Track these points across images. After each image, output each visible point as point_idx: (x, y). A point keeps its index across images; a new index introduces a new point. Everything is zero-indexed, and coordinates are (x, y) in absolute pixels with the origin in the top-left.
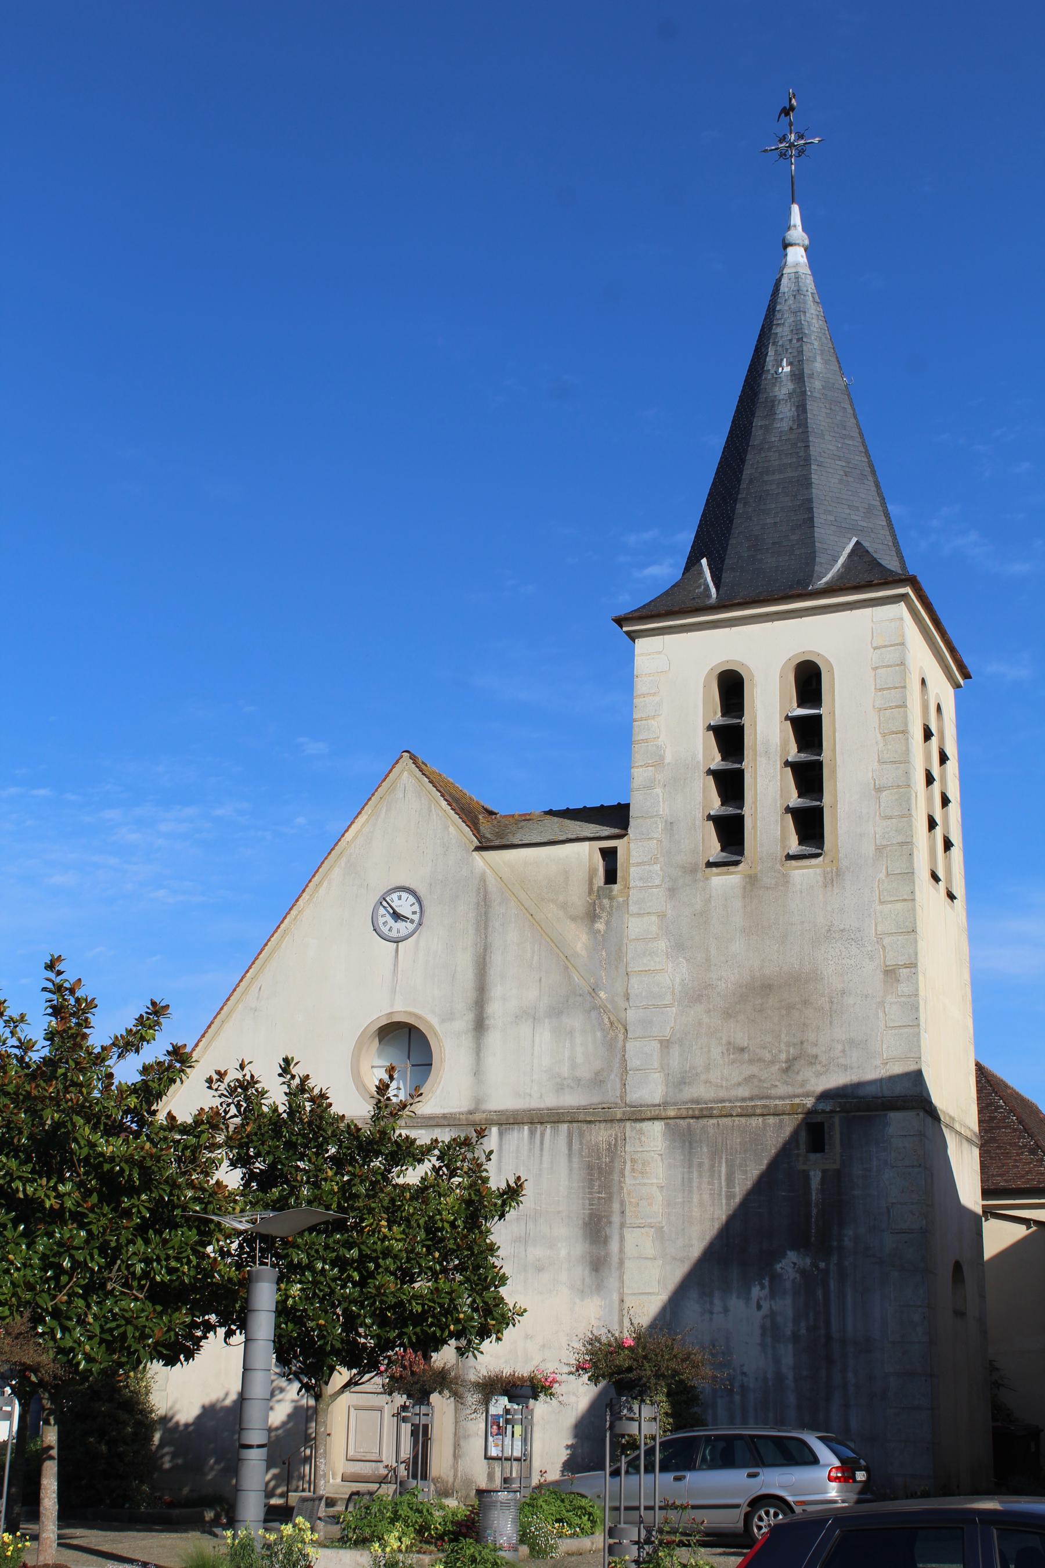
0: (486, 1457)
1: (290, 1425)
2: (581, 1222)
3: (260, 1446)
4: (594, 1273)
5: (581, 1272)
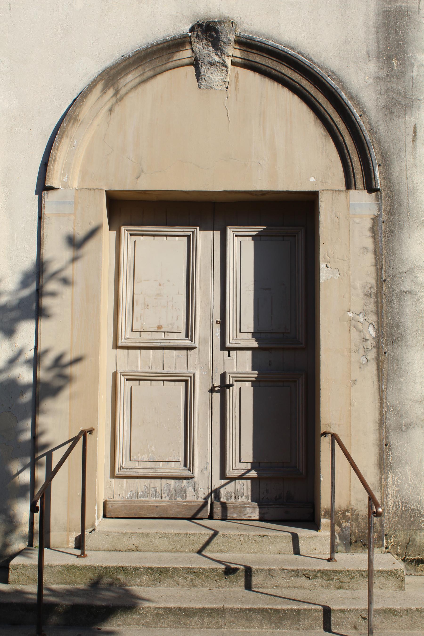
3: (18, 473)
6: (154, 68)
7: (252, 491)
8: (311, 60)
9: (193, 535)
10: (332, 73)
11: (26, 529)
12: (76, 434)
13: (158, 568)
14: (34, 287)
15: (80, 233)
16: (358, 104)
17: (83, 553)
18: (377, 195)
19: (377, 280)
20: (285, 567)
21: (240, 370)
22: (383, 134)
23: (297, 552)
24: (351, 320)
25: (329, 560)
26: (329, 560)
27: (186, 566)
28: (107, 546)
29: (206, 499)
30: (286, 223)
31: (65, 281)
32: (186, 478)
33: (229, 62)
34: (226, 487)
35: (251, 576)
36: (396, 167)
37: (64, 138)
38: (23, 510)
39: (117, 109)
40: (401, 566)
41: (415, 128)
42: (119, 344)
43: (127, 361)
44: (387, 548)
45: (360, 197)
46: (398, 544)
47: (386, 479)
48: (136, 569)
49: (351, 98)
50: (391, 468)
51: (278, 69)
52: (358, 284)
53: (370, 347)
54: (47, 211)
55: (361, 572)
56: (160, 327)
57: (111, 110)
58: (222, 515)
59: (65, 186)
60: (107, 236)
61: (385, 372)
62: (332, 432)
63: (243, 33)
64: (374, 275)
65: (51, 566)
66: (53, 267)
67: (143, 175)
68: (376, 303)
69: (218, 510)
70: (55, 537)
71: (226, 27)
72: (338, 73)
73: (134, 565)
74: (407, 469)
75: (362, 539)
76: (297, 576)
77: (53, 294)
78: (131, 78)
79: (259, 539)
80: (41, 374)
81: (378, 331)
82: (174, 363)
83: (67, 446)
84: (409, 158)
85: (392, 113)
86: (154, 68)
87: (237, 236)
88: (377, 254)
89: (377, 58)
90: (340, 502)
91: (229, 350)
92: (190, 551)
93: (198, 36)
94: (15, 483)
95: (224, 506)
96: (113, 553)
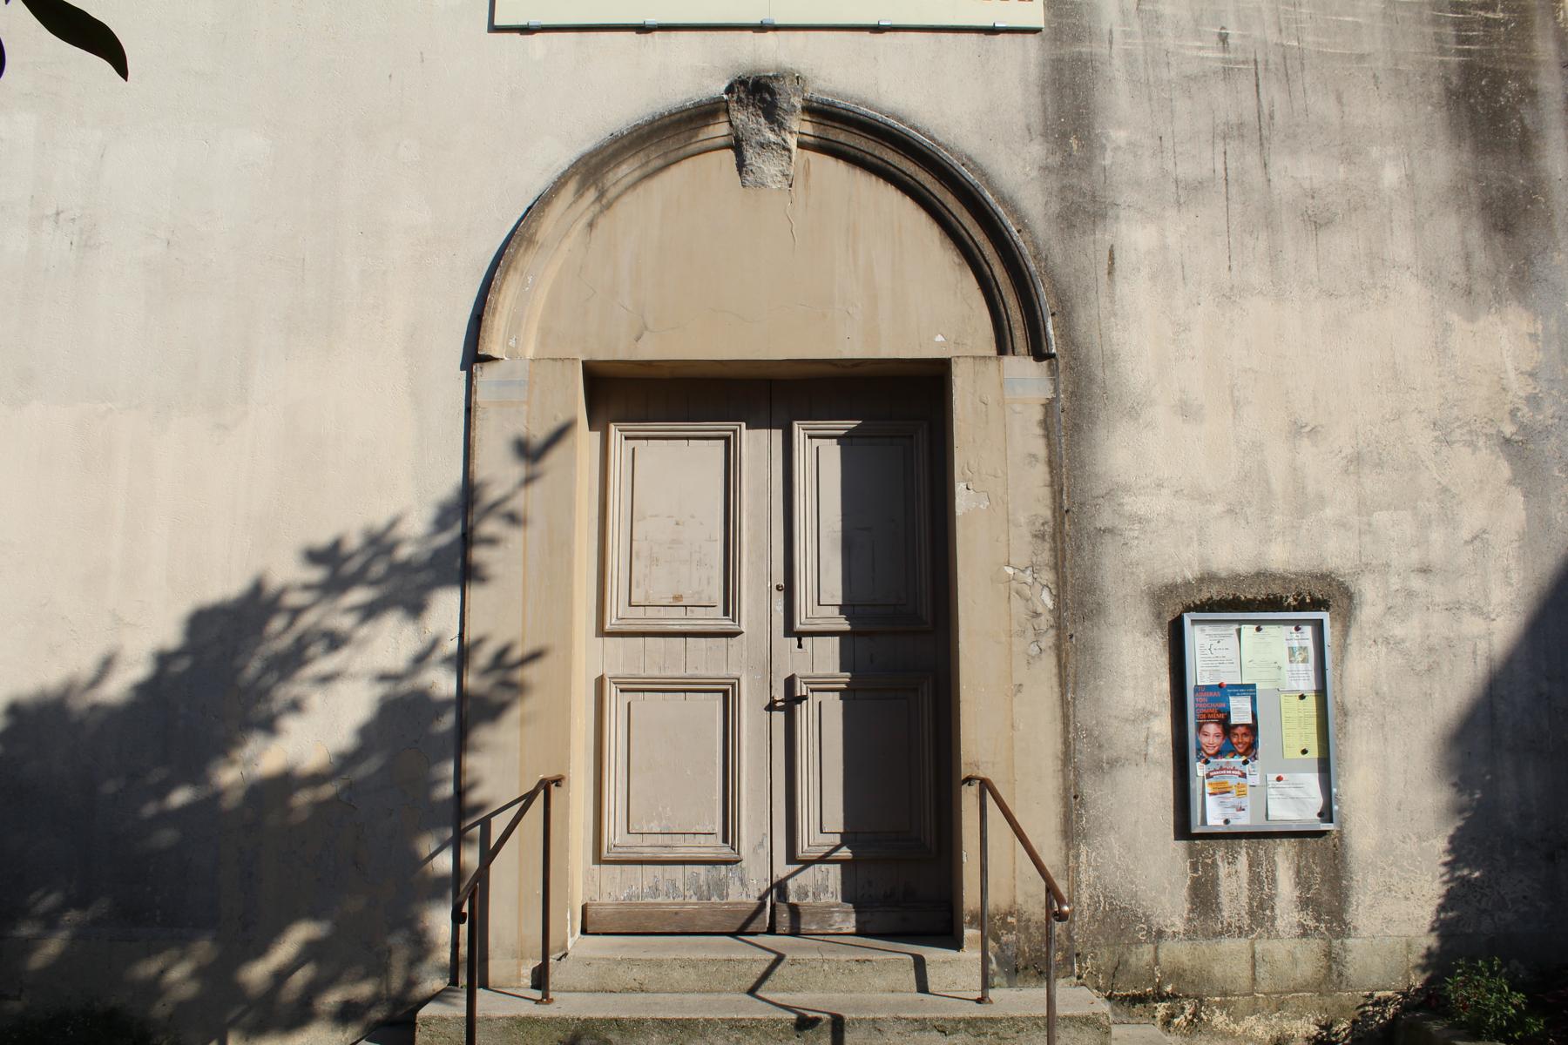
0: (1183, 829)
1: (364, 770)
2: (1436, 88)
3: (432, 856)
4: (1499, 239)
5: (1453, 232)
6: (665, 154)
7: (843, 883)
8: (932, 138)
9: (741, 962)
10: (969, 161)
11: (445, 955)
12: (530, 787)
13: (678, 1020)
14: (457, 530)
15: (539, 434)
16: (1014, 210)
17: (545, 996)
18: (1050, 365)
19: (1054, 512)
20: (902, 1015)
21: (819, 672)
22: (1058, 261)
23: (923, 987)
24: (1010, 579)
25: (979, 1001)
26: (979, 1001)
27: (728, 1016)
28: (588, 984)
29: (762, 898)
30: (895, 415)
31: (513, 519)
32: (726, 863)
33: (792, 142)
34: (798, 877)
35: (842, 1031)
36: (1083, 318)
37: (511, 272)
38: (439, 921)
39: (602, 222)
40: (1104, 1007)
41: (1111, 252)
42: (608, 627)
43: (621, 658)
44: (1079, 977)
45: (1022, 367)
46: (1098, 970)
47: (1077, 857)
48: (639, 1022)
49: (1003, 200)
50: (1085, 837)
51: (877, 153)
52: (1022, 518)
53: (1044, 627)
54: (480, 397)
55: (1034, 1020)
56: (678, 598)
57: (591, 225)
58: (792, 927)
59: (513, 354)
60: (585, 440)
61: (1071, 671)
62: (982, 775)
63: (816, 95)
64: (1048, 501)
65: (489, 1020)
66: (492, 494)
67: (646, 334)
68: (1054, 550)
69: (784, 917)
70: (498, 967)
71: (787, 85)
72: (979, 160)
73: (636, 1016)
74: (1112, 838)
75: (1036, 963)
76: (923, 1029)
77: (492, 541)
78: (626, 171)
79: (856, 968)
80: (471, 681)
81: (1058, 598)
82: (704, 659)
83: (517, 807)
84: (1103, 301)
85: (1072, 226)
86: (665, 154)
87: (810, 437)
88: (1053, 464)
89: (1044, 135)
90: (998, 899)
91: (800, 635)
92: (734, 991)
93: (739, 101)
94: (425, 874)
95: (794, 911)
96: (598, 995)
